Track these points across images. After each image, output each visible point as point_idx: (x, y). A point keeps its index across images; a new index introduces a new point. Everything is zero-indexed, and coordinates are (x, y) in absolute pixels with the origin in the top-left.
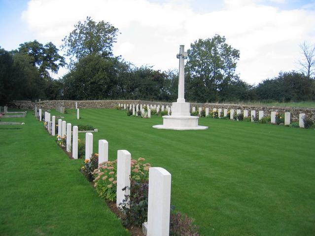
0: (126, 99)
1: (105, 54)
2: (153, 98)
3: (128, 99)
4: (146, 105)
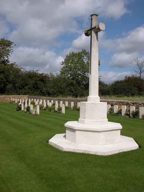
0: (18, 95)
1: (4, 62)
2: (39, 94)
3: (19, 95)
4: (19, 100)
